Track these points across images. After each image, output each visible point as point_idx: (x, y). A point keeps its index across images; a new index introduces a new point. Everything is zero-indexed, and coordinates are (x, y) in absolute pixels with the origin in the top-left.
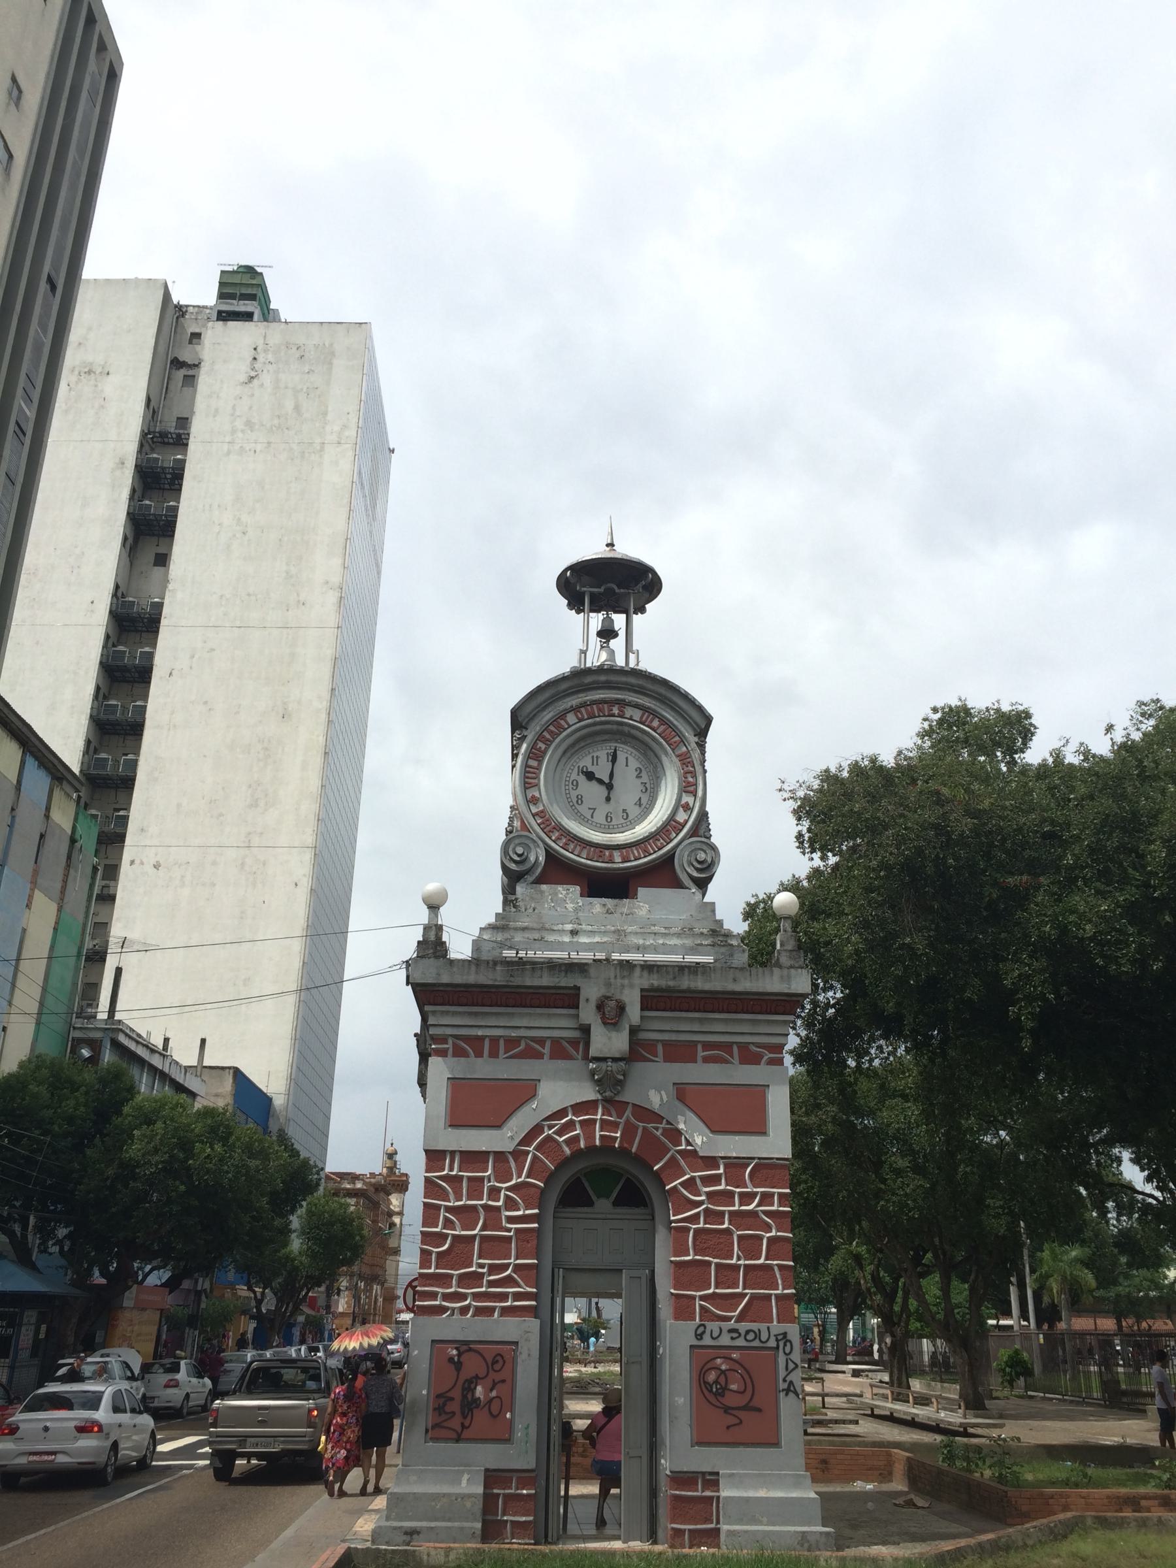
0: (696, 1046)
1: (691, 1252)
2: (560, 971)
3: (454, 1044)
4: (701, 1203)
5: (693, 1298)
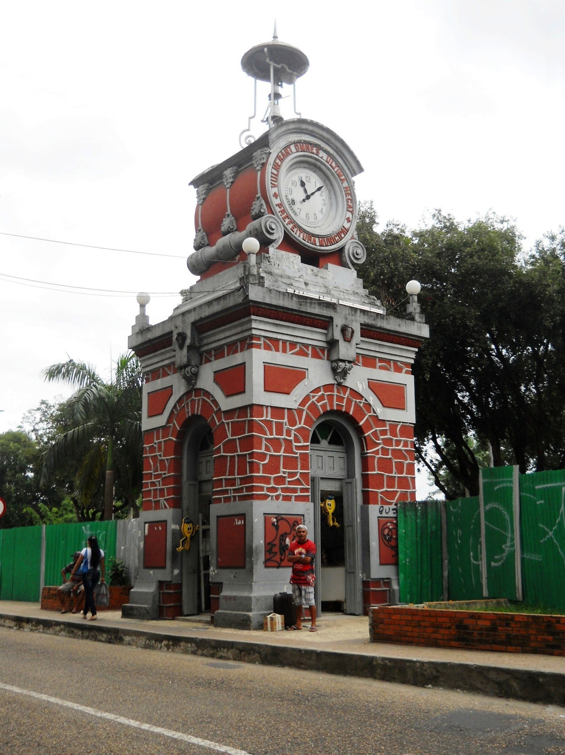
0: (376, 359)
1: (376, 469)
2: (324, 306)
3: (264, 342)
4: (379, 444)
5: (377, 493)
